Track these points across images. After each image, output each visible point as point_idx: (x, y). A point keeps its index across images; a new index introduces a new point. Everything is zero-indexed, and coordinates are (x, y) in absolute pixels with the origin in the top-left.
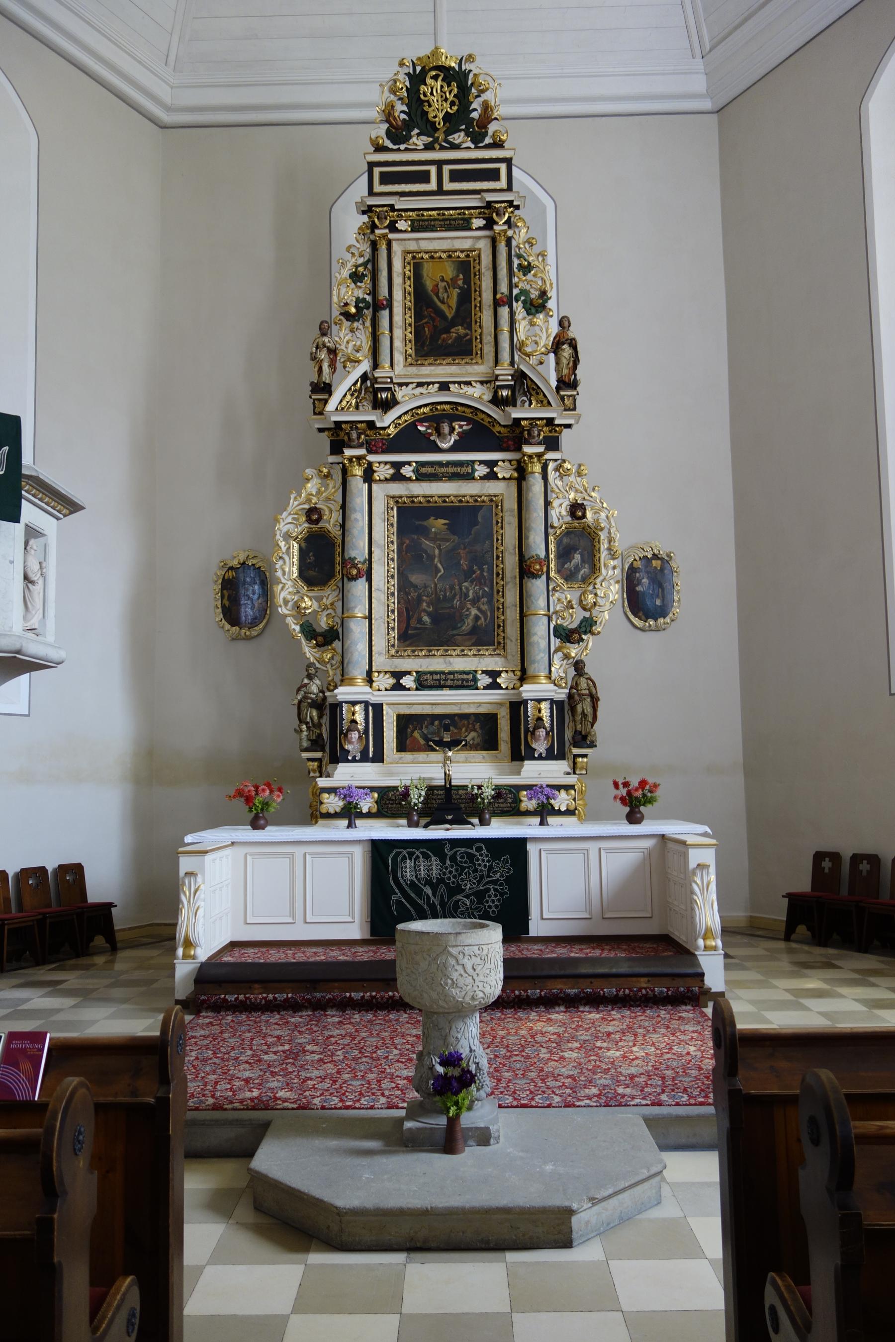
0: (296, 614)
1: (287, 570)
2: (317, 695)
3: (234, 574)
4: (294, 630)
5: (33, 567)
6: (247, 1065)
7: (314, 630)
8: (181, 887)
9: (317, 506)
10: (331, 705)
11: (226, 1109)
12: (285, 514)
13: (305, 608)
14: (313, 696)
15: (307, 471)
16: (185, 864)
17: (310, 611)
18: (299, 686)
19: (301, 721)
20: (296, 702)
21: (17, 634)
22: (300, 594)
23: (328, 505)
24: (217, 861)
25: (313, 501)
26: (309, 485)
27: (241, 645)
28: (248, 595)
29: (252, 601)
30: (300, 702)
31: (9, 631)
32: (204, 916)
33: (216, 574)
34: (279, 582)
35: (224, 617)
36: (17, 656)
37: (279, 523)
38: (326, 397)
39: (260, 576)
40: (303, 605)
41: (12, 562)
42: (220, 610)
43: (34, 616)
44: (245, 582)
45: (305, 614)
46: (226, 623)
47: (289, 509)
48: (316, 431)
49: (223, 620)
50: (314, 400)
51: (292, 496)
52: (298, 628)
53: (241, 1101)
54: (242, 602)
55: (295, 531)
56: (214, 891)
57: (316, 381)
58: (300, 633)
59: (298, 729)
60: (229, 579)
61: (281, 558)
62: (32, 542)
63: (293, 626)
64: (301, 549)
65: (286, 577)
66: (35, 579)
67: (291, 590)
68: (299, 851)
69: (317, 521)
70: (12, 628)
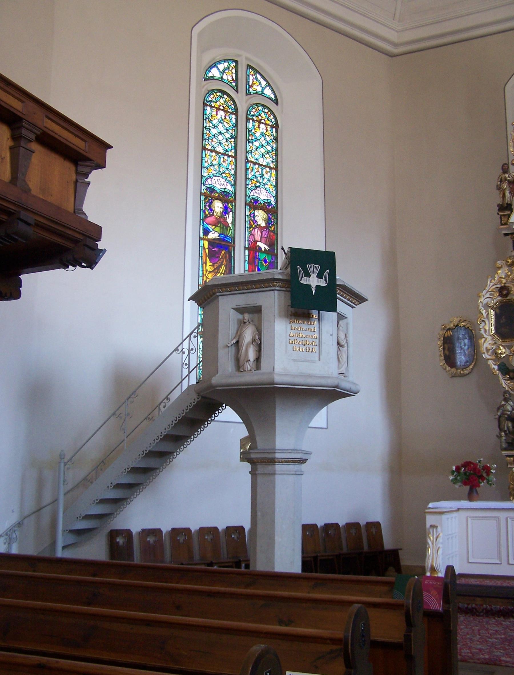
0: (494, 358)
1: (487, 328)
2: (511, 412)
3: (451, 333)
4: (494, 368)
5: (342, 337)
6: (479, 643)
7: (508, 369)
8: (427, 535)
9: (506, 285)
10: (303, 570)
11: (469, 662)
12: (484, 292)
13: (501, 354)
14: (509, 413)
15: (498, 262)
16: (430, 520)
17: (504, 355)
18: (498, 406)
19: (501, 429)
20: (497, 417)
21: (335, 376)
22: (497, 345)
23: (512, 283)
24: (450, 520)
25: (504, 282)
26: (499, 272)
27: (457, 380)
28: (461, 347)
29: (464, 350)
30: (500, 417)
31: (331, 375)
32: (442, 554)
33: (439, 334)
34: (482, 337)
35: (446, 362)
36: (336, 389)
37: (481, 297)
38: (509, 213)
39: (468, 334)
40: (500, 352)
41: (331, 335)
42: (442, 358)
43: (343, 366)
44: (458, 338)
45: (501, 358)
46: (447, 366)
47: (487, 288)
48: (503, 236)
49: (445, 364)
50: (501, 215)
51: (489, 280)
52: (496, 367)
53: (479, 659)
54: (457, 352)
55: (492, 302)
56: (448, 539)
57: (501, 203)
58: (498, 370)
59: (499, 435)
60: (448, 336)
61: (483, 321)
62: (340, 322)
63: (493, 366)
64: (496, 315)
65: (487, 333)
66: (343, 344)
67: (490, 342)
68: (502, 515)
69: (507, 295)
70: (332, 373)
